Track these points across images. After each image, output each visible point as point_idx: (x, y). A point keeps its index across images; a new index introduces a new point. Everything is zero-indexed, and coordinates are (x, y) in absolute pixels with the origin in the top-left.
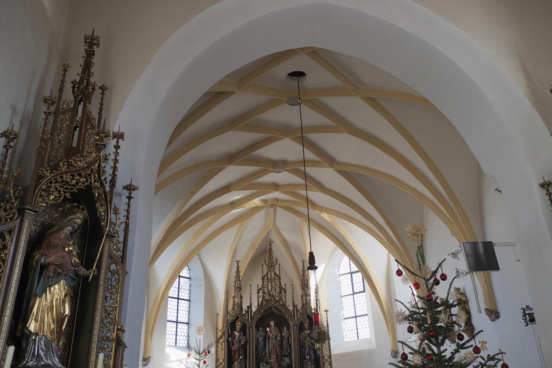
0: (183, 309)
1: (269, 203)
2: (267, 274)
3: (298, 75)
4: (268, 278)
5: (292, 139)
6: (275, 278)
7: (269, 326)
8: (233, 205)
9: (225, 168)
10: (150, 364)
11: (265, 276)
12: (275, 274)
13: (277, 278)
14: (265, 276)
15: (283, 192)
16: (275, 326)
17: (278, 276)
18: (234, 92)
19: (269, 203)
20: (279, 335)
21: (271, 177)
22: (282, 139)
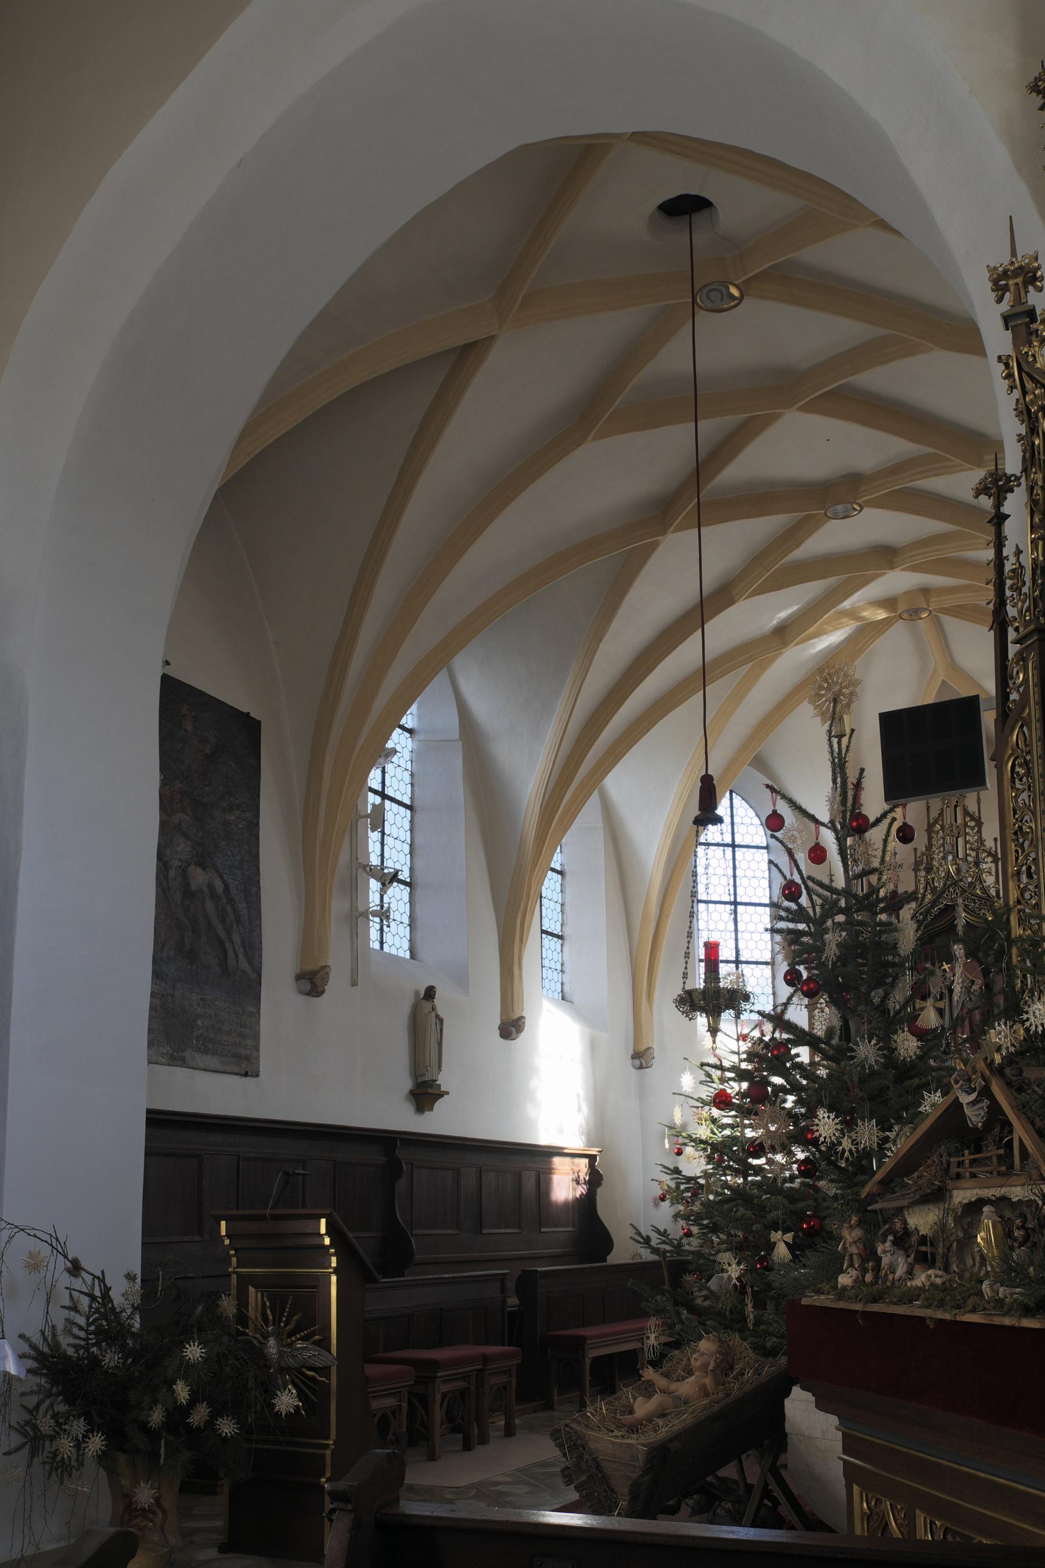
0: (751, 927)
1: (901, 607)
2: (941, 814)
3: (685, 208)
4: (943, 828)
5: (807, 409)
6: (966, 825)
7: (950, 958)
8: (783, 634)
9: (655, 545)
10: (656, 1063)
11: (936, 821)
12: (966, 813)
13: (973, 824)
14: (936, 821)
15: (914, 569)
16: (968, 955)
17: (973, 818)
18: (492, 339)
19: (901, 607)
20: (979, 982)
21: (834, 536)
22: (778, 416)
